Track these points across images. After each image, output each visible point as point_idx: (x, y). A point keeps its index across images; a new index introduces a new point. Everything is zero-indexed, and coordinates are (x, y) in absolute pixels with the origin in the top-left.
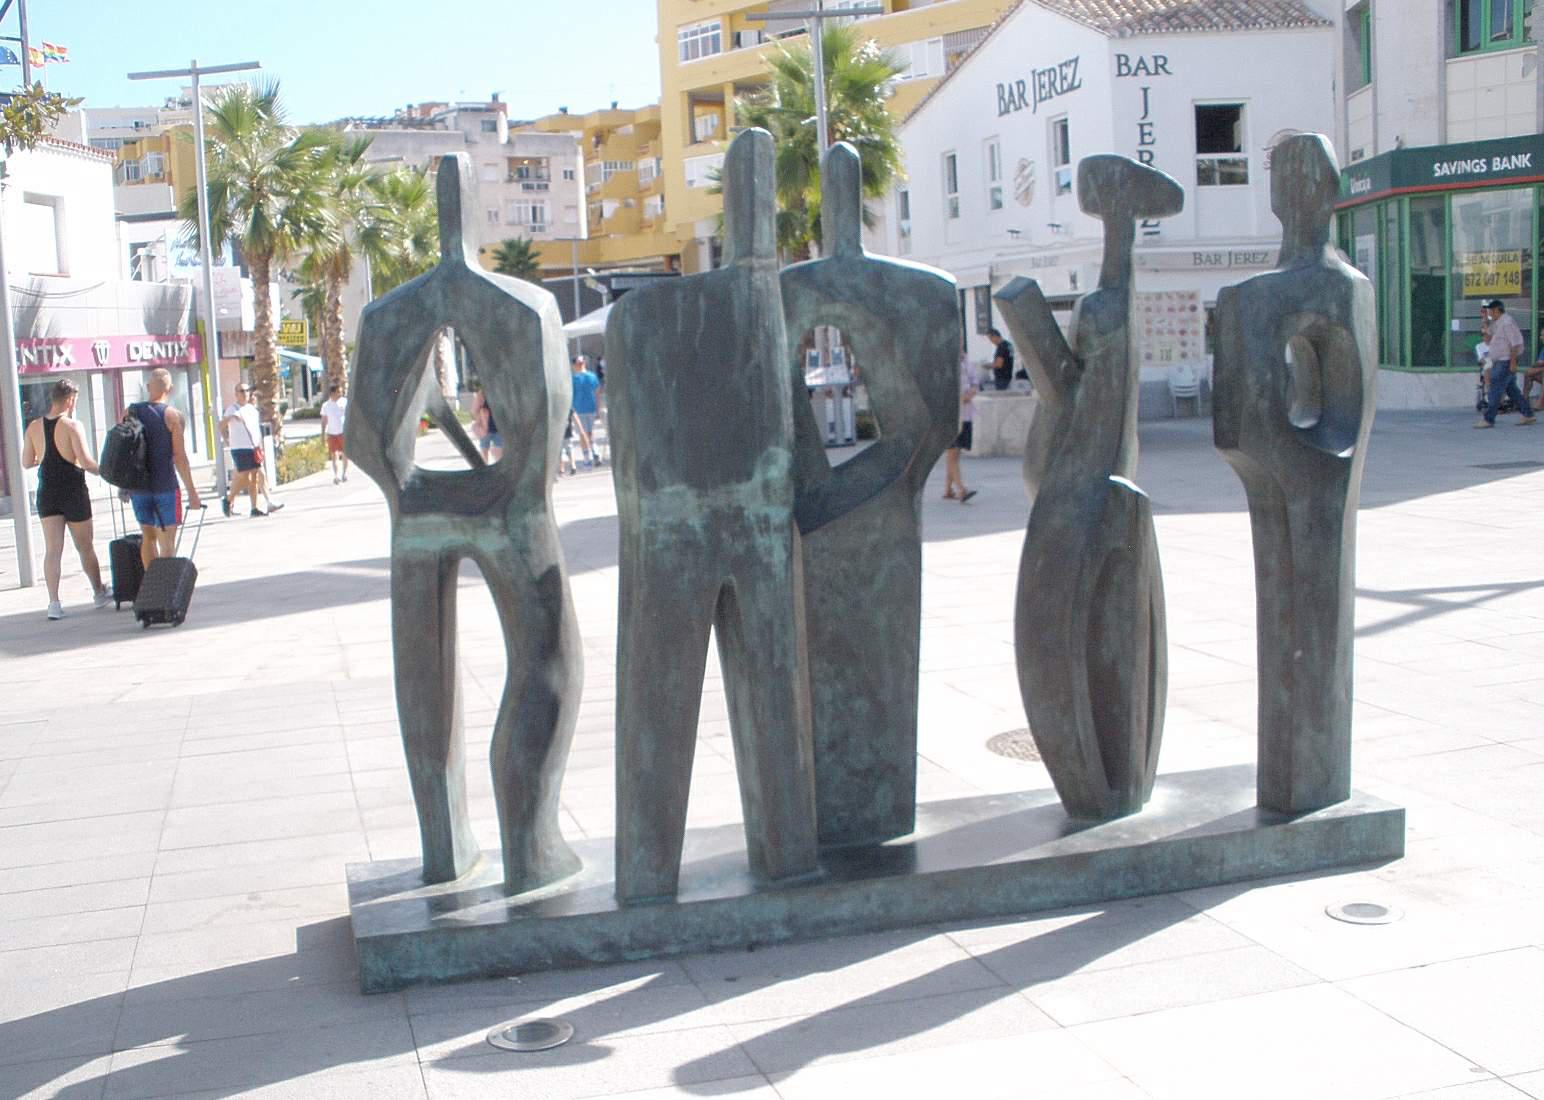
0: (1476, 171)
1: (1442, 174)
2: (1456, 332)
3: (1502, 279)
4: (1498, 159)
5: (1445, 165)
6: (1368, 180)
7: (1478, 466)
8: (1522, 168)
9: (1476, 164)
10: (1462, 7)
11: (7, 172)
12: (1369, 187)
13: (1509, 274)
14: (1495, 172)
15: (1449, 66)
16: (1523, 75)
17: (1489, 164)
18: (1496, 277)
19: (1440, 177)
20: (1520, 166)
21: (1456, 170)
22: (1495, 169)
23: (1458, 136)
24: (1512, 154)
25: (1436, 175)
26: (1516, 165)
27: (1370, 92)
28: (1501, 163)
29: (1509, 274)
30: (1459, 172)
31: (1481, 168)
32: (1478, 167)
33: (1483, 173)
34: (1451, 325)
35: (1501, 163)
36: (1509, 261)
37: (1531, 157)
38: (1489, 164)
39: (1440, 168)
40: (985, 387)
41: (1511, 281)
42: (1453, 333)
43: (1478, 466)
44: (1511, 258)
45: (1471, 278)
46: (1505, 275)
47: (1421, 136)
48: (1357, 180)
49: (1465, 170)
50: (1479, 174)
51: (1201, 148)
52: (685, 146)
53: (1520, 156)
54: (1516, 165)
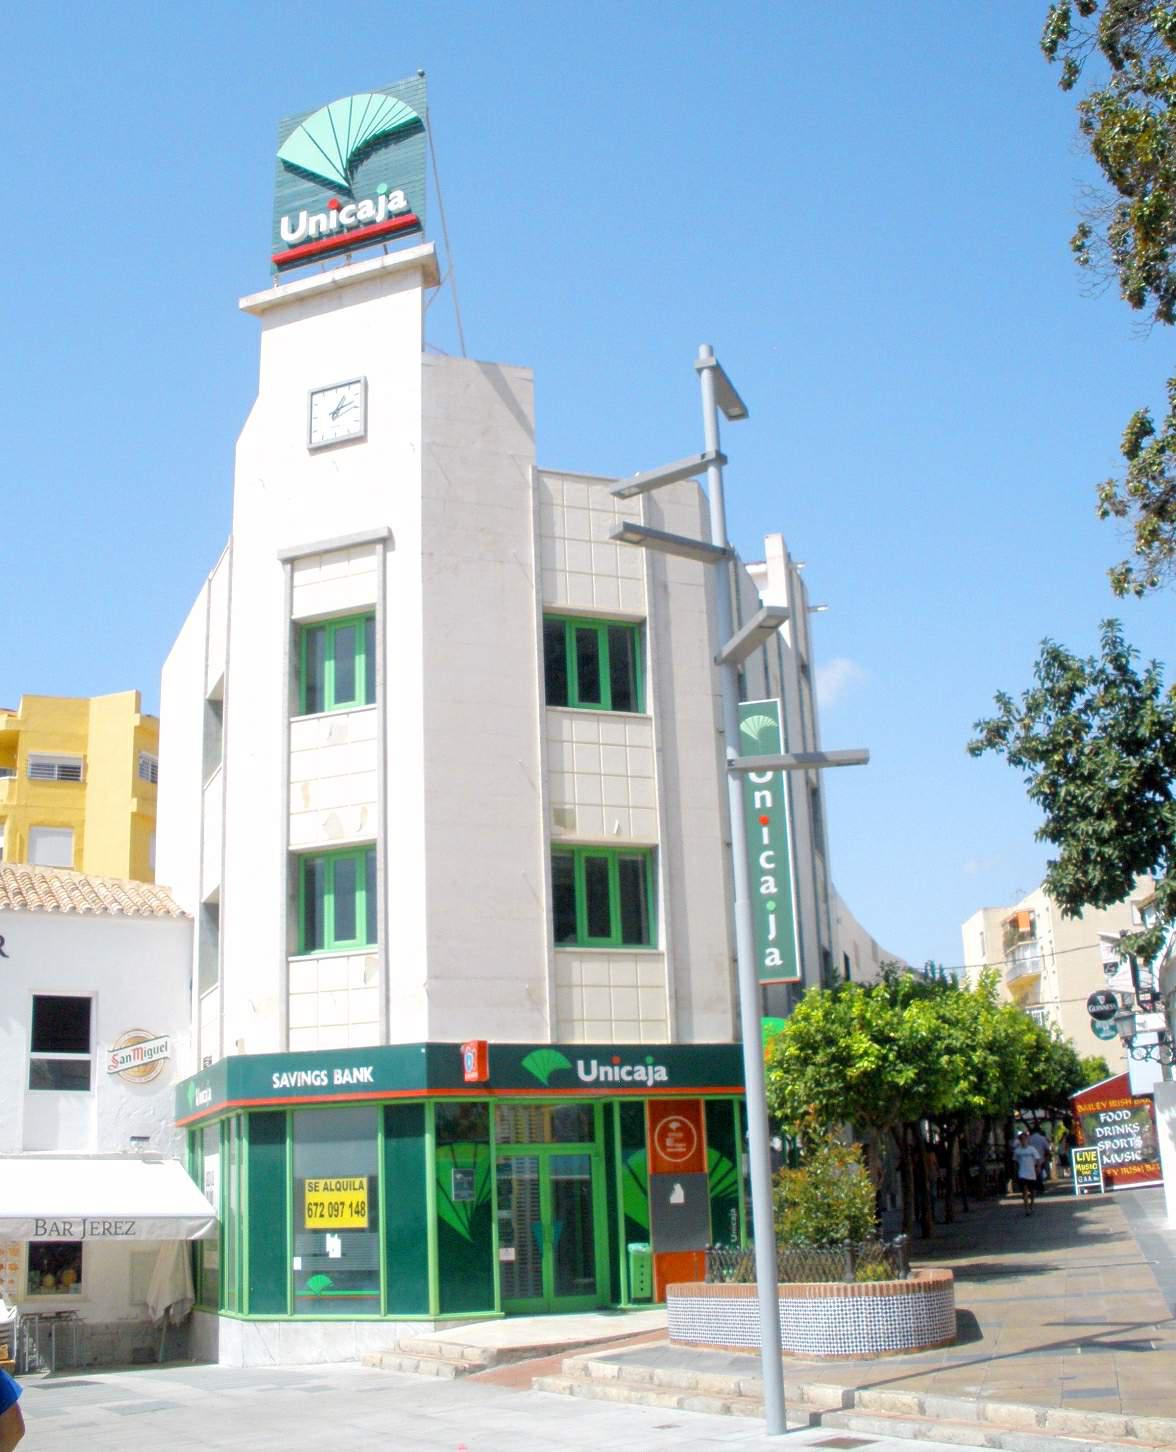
0: (317, 1083)
1: (344, 1082)
2: (298, 1271)
3: (347, 1210)
4: (340, 1071)
5: (285, 1075)
6: (210, 1090)
7: (1027, 1351)
8: (364, 1083)
9: (317, 1076)
10: (733, 877)
11: (1087, 909)
12: (210, 1098)
13: (354, 1205)
14: (337, 1086)
15: (291, 964)
16: (365, 981)
17: (330, 1076)
18: (340, 1207)
19: (279, 1089)
20: (362, 1080)
21: (296, 1084)
22: (336, 1082)
23: (301, 1044)
24: (337, 1067)
25: (275, 1086)
26: (358, 1079)
27: (217, 992)
28: (343, 1075)
29: (354, 1205)
30: (299, 1085)
31: (322, 1080)
32: (318, 1079)
33: (325, 1087)
34: (292, 1262)
35: (343, 1075)
36: (354, 1189)
37: (373, 1071)
38: (330, 1076)
39: (280, 1079)
40: (166, 1290)
41: (357, 1212)
42: (295, 1273)
43: (1027, 1351)
44: (357, 1186)
45: (314, 1208)
46: (351, 1206)
47: (265, 1043)
48: (202, 1090)
49: (305, 1082)
50: (321, 1086)
51: (39, 1044)
52: (97, 993)
53: (361, 1069)
54: (358, 1079)
